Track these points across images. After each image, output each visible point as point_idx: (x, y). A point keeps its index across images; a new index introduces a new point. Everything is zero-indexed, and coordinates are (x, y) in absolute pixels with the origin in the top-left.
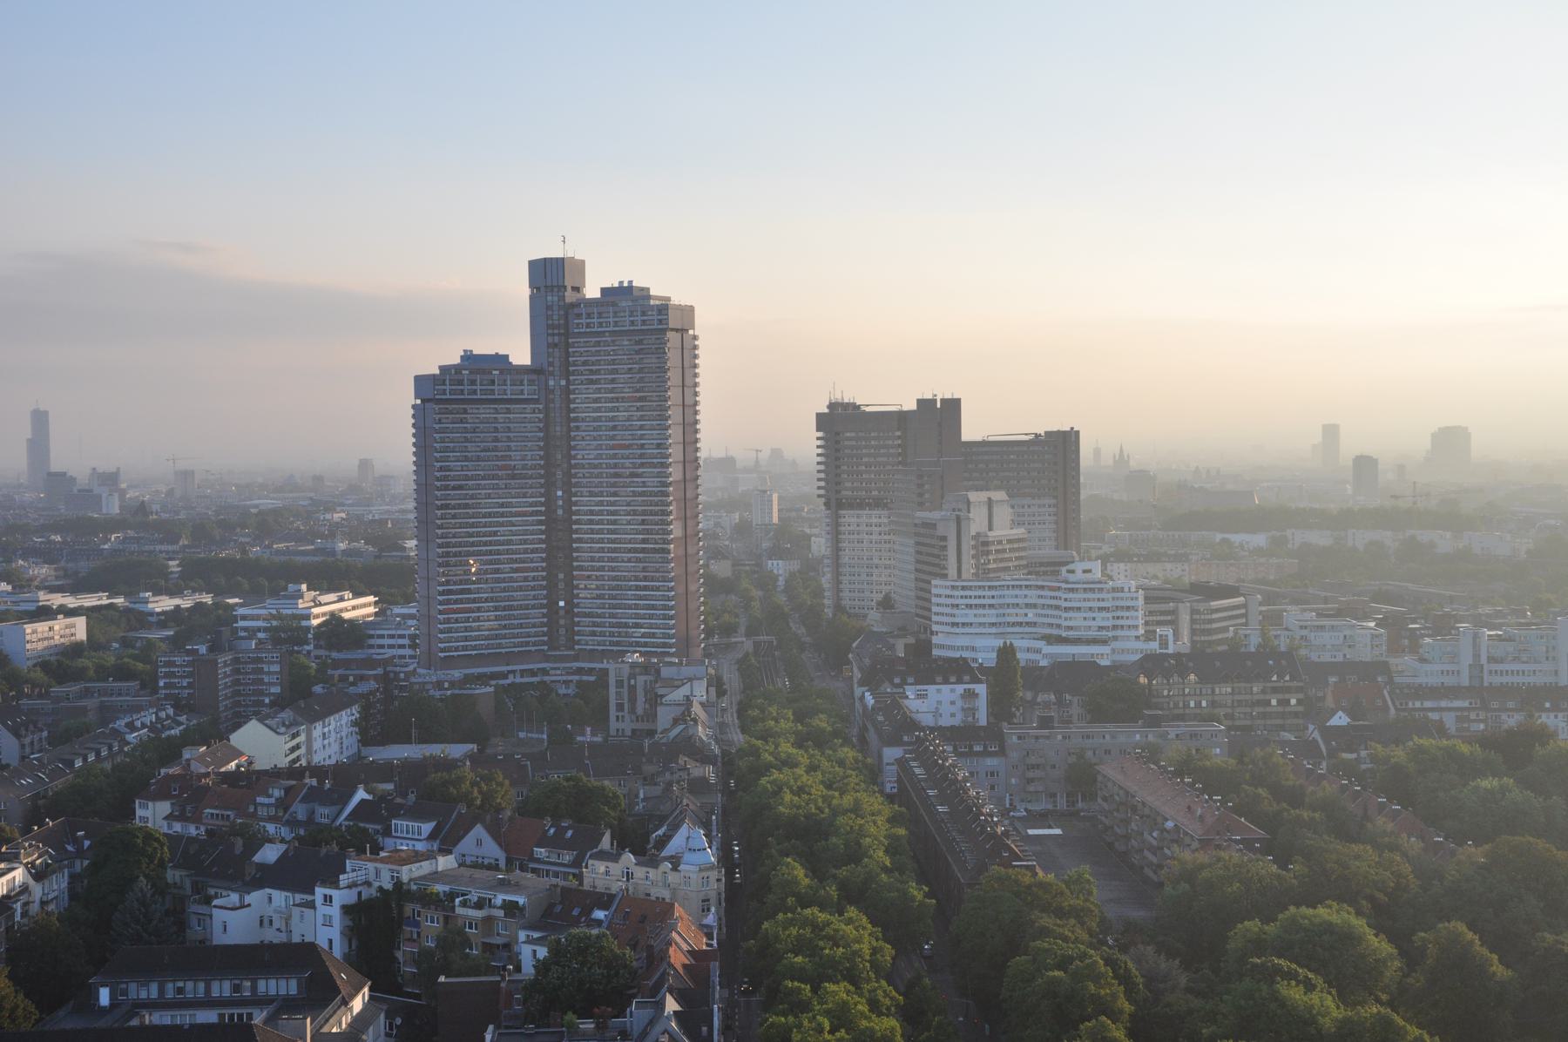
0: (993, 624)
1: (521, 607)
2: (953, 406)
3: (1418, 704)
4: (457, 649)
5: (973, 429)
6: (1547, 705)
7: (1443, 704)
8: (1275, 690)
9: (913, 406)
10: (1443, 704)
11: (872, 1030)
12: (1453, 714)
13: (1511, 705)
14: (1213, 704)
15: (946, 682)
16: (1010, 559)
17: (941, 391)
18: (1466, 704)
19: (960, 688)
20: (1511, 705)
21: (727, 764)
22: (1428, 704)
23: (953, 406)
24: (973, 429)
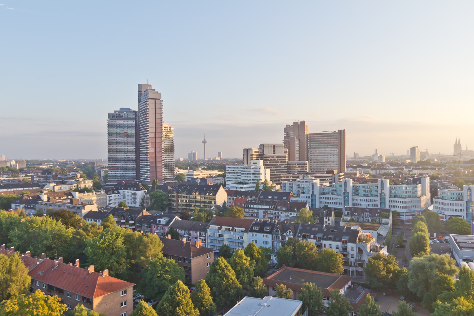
0: (235, 178)
1: (130, 169)
2: (303, 123)
3: (252, 206)
4: (113, 178)
5: (309, 130)
6: (296, 210)
7: (260, 207)
8: (207, 198)
9: (292, 124)
10: (260, 207)
11: (58, 297)
12: (262, 211)
13: (284, 209)
14: (190, 201)
15: (130, 190)
16: (278, 162)
17: (299, 119)
18: (268, 207)
19: (133, 192)
20: (284, 209)
21: (375, 216)
22: (255, 206)
23: (303, 123)
24: (309, 130)
